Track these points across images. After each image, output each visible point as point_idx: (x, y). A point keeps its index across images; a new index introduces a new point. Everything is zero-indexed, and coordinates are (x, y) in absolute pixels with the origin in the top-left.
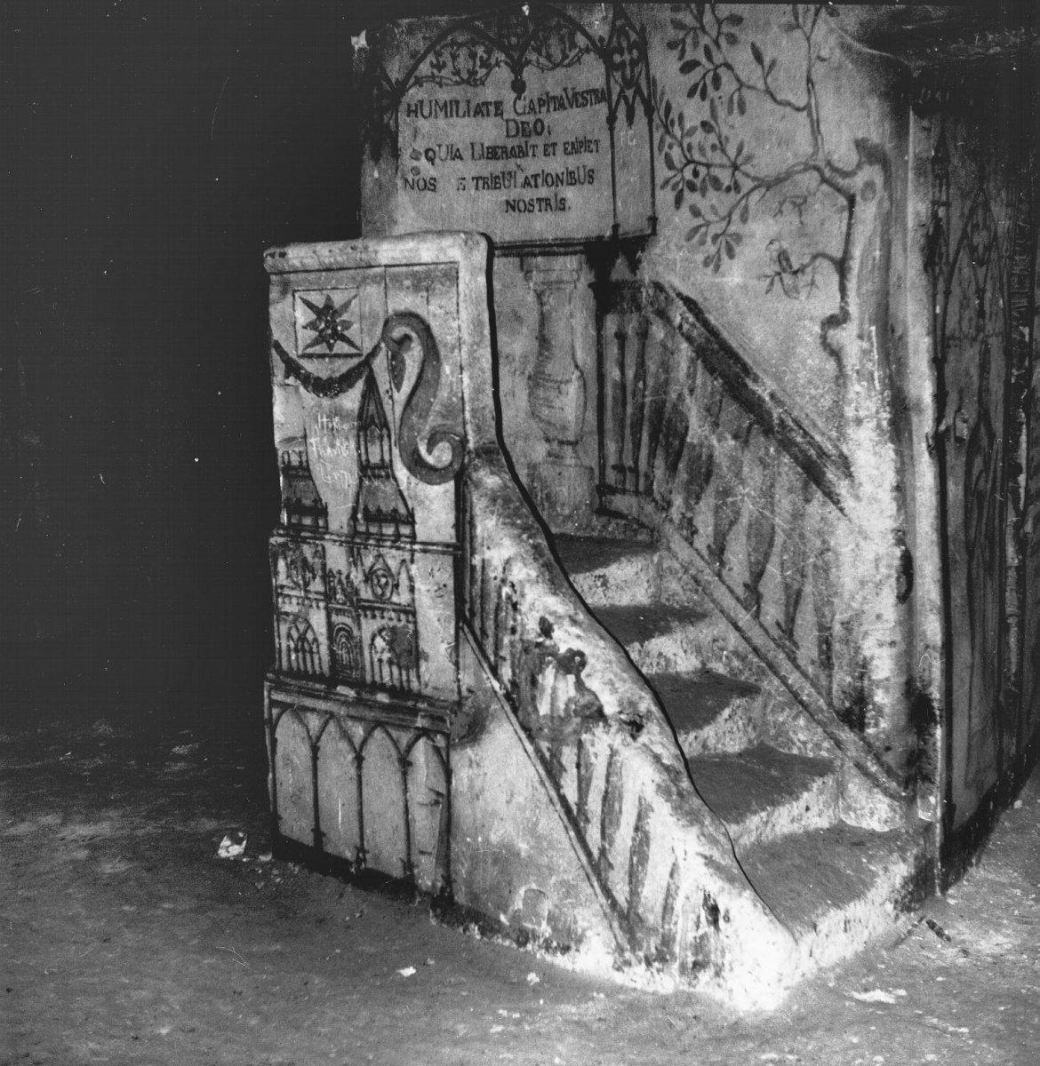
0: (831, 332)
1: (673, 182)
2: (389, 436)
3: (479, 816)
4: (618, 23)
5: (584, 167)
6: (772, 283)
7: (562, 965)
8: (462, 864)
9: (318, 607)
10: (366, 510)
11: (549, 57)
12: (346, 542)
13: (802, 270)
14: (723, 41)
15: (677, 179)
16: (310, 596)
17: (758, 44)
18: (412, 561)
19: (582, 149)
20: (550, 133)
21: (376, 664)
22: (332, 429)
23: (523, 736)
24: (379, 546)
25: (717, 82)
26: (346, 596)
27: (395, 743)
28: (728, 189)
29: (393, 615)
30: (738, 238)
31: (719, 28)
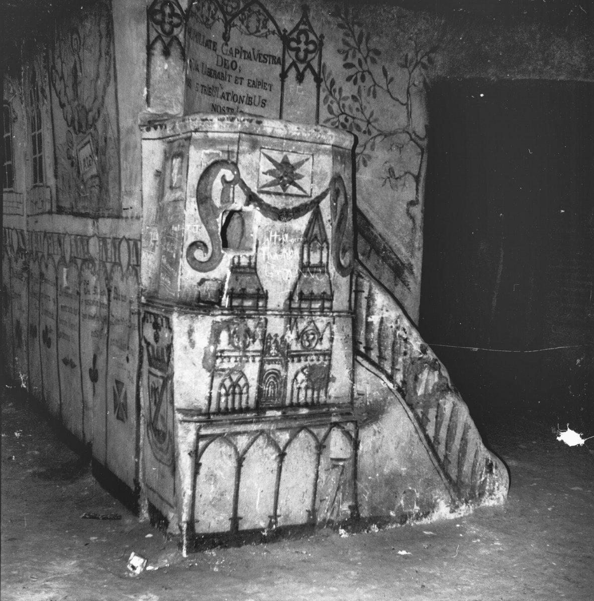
0: (411, 208)
1: (332, 121)
2: (328, 248)
3: (377, 461)
4: (302, 27)
5: (260, 97)
6: (385, 182)
7: (425, 523)
8: (366, 494)
9: (254, 361)
10: (301, 294)
11: (247, 27)
12: (284, 315)
13: (400, 178)
14: (369, 60)
15: (335, 120)
16: (248, 354)
17: (386, 68)
18: (334, 323)
19: (260, 87)
20: (240, 71)
21: (296, 391)
22: (281, 241)
23: (408, 409)
24: (312, 316)
25: (363, 79)
26: (278, 351)
27: (315, 437)
28: (365, 132)
29: (314, 357)
30: (370, 157)
31: (368, 53)
